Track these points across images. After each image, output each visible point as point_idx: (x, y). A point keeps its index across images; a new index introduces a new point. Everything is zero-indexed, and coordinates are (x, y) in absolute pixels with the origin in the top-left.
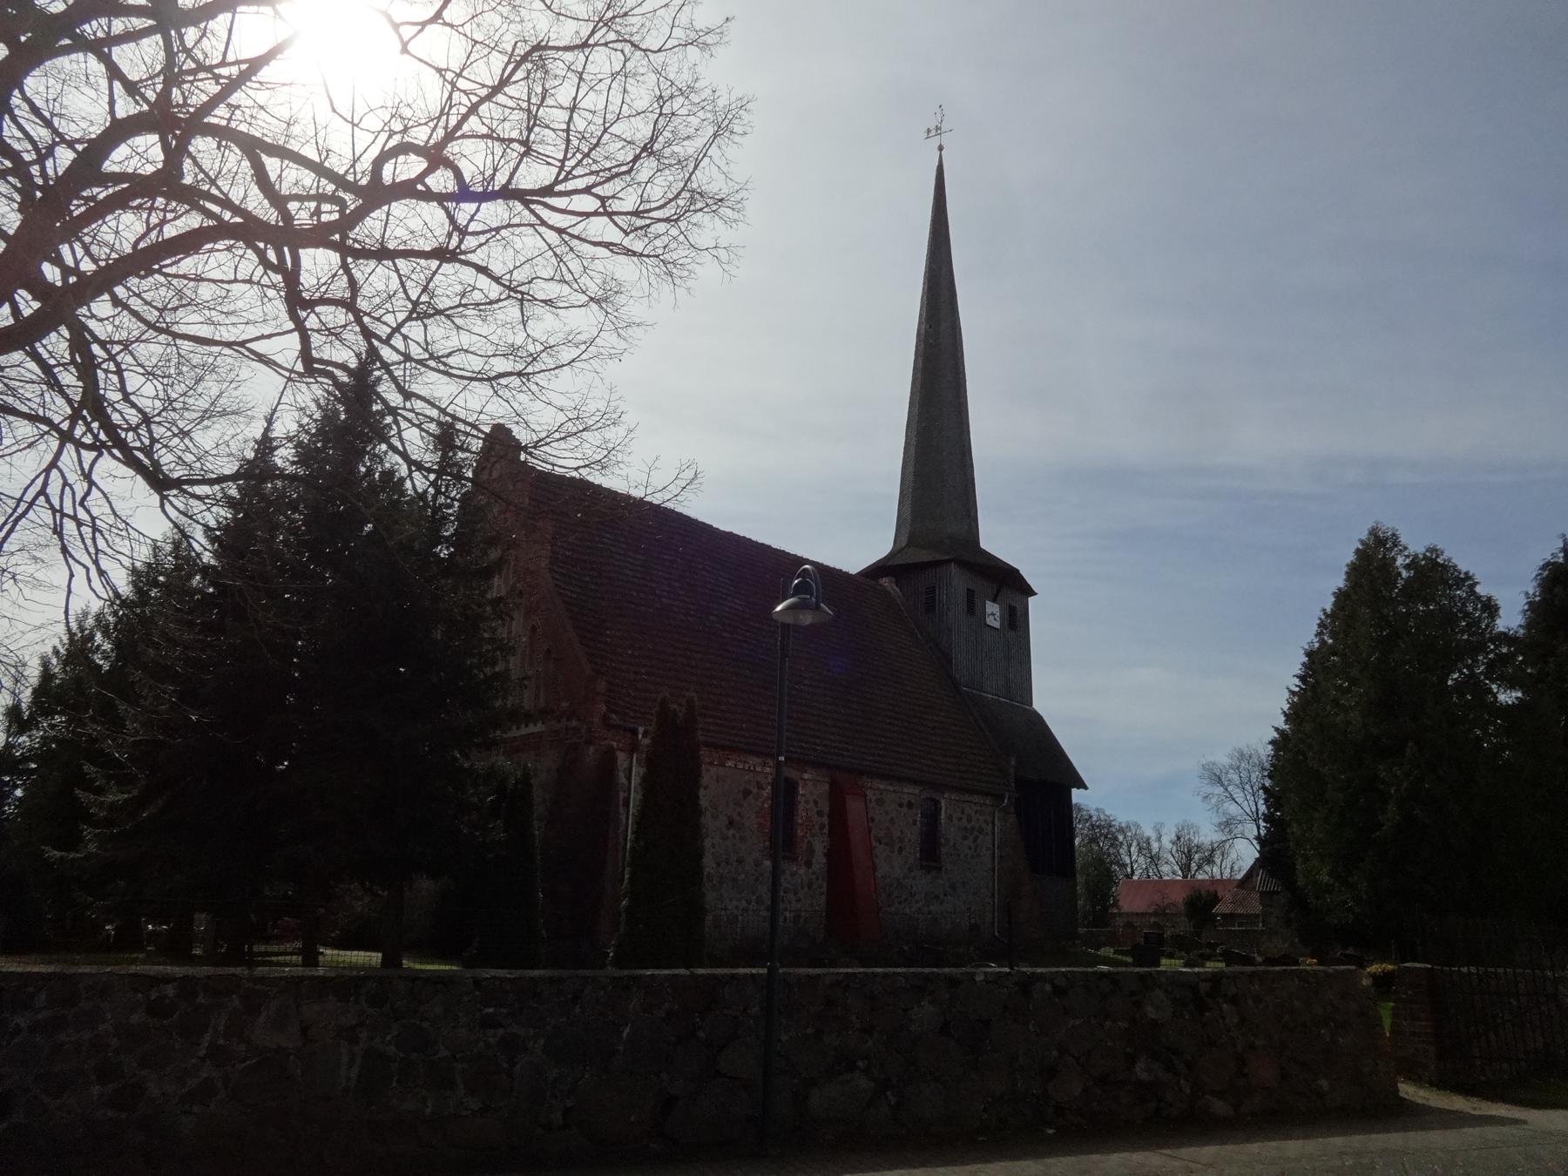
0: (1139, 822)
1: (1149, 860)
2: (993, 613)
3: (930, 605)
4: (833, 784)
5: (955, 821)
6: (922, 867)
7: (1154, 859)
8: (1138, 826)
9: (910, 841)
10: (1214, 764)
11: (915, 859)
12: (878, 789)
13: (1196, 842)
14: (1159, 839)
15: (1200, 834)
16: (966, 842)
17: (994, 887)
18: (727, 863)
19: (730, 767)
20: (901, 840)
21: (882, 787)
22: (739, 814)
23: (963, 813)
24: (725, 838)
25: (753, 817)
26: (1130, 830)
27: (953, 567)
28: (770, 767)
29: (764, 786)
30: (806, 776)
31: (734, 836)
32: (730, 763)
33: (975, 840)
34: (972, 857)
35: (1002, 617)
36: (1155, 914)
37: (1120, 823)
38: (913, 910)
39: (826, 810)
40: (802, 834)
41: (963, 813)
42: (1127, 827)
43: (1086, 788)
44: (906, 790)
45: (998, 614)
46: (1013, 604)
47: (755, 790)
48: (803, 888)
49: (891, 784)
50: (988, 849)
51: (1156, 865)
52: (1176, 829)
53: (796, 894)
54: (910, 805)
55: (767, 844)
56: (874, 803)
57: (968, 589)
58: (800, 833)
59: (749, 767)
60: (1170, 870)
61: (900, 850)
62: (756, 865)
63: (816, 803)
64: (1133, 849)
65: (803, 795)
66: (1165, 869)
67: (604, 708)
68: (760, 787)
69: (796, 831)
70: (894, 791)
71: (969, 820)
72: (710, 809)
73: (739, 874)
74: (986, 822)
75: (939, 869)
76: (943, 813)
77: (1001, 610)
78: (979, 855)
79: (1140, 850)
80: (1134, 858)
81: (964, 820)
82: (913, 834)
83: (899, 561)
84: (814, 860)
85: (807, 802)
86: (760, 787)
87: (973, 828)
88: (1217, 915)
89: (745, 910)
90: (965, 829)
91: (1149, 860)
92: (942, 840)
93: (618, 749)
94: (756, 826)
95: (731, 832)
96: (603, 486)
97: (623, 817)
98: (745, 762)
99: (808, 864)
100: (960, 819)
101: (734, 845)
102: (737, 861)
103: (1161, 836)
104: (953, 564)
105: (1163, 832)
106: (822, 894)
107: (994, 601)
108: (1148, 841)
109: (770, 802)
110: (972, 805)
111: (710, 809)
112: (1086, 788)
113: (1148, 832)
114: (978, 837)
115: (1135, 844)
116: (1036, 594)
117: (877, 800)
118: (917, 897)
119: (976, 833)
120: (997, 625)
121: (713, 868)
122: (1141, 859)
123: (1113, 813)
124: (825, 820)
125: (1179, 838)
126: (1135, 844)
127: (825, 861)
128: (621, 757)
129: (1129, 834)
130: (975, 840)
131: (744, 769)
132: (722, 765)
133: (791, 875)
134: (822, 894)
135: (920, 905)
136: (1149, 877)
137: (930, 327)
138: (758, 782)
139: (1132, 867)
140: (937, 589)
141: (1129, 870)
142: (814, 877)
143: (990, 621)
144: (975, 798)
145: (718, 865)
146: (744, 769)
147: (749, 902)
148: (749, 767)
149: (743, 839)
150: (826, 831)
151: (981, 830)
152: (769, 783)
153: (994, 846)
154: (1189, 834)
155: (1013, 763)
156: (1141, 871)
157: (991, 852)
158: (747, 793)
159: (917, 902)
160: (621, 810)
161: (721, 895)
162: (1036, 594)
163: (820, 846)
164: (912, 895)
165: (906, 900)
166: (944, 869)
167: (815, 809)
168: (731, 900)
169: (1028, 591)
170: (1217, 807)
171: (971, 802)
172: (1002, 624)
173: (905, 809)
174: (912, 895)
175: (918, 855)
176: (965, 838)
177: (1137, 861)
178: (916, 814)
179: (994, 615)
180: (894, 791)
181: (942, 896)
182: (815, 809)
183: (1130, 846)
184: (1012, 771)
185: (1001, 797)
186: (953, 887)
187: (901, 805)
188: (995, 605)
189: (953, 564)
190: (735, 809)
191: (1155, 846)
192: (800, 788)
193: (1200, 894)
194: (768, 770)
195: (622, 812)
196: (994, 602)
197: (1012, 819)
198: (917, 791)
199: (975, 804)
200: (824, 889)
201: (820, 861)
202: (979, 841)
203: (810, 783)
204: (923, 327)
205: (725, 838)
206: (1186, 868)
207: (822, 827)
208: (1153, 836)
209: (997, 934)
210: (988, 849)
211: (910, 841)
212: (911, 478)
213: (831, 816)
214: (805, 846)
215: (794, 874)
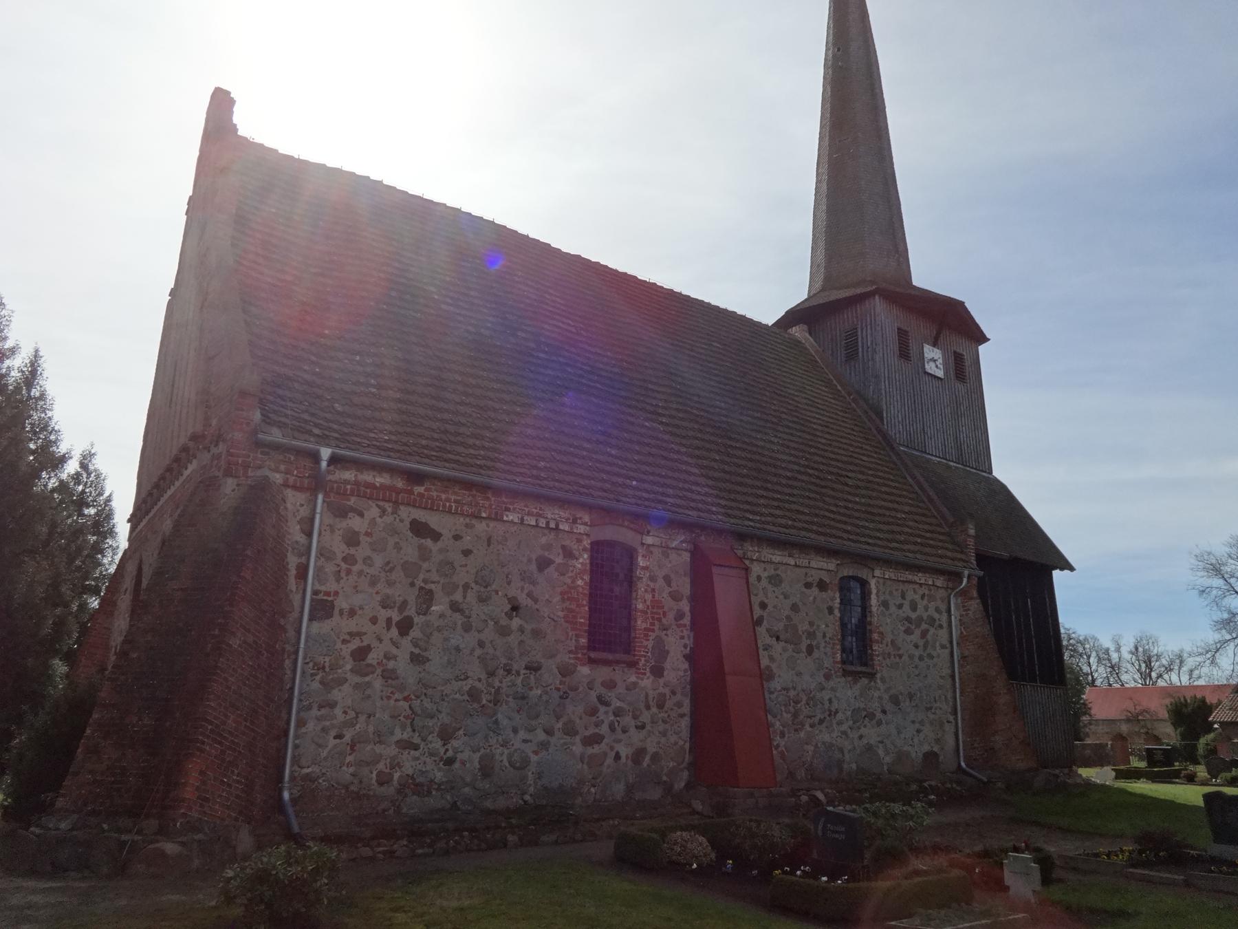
0: (1096, 635)
1: (1109, 670)
2: (934, 359)
3: (852, 352)
4: (697, 555)
5: (893, 609)
6: (846, 673)
7: (1114, 668)
8: (1096, 639)
9: (824, 636)
10: (1209, 554)
11: (835, 662)
12: (771, 562)
13: (1155, 652)
14: (1118, 650)
15: (1160, 644)
16: (909, 638)
17: (955, 698)
18: (509, 672)
19: (512, 522)
20: (811, 635)
21: (777, 559)
22: (529, 595)
23: (903, 597)
24: (504, 632)
25: (557, 599)
26: (1088, 642)
27: (878, 304)
28: (585, 524)
29: (576, 553)
30: (649, 540)
31: (521, 630)
32: (511, 517)
33: (924, 634)
34: (921, 658)
35: (945, 364)
36: (1128, 720)
37: (1079, 636)
38: (834, 735)
39: (686, 590)
40: (644, 626)
41: (903, 597)
42: (1084, 640)
43: (1072, 569)
44: (813, 564)
45: (940, 361)
46: (960, 351)
47: (559, 560)
48: (648, 707)
49: (790, 556)
50: (943, 647)
51: (1117, 674)
52: (1134, 640)
53: (635, 717)
54: (822, 586)
55: (583, 641)
56: (764, 582)
57: (898, 329)
58: (640, 624)
59: (548, 523)
60: (1130, 678)
61: (810, 650)
62: (563, 676)
63: (667, 580)
64: (1092, 660)
65: (646, 568)
66: (1124, 677)
67: (257, 416)
68: (568, 554)
69: (636, 622)
70: (796, 566)
71: (914, 607)
72: (473, 585)
73: (531, 689)
74: (937, 610)
75: (871, 676)
76: (873, 596)
77: (944, 356)
78: (931, 657)
79: (1099, 660)
80: (1094, 667)
81: (906, 607)
82: (829, 626)
83: (814, 302)
84: (667, 665)
85: (653, 579)
86: (568, 554)
87: (920, 619)
88: (1215, 723)
89: (544, 746)
90: (908, 619)
91: (1109, 670)
92: (875, 636)
93: (286, 485)
94: (561, 614)
95: (516, 622)
96: (385, 183)
97: (296, 599)
98: (540, 515)
99: (658, 672)
100: (900, 606)
101: (522, 642)
102: (527, 668)
103: (1120, 647)
104: (877, 297)
105: (1122, 643)
106: (682, 716)
107: (935, 344)
108: (1107, 651)
109: (587, 578)
110: (916, 586)
111: (473, 585)
112: (1072, 569)
113: (1106, 642)
114: (927, 631)
115: (1094, 654)
116: (989, 340)
117: (770, 578)
118: (840, 716)
119: (924, 626)
120: (940, 373)
121: (480, 680)
122: (1101, 669)
123: (1072, 627)
124: (685, 606)
125: (1137, 649)
126: (1094, 654)
127: (686, 666)
128: (294, 501)
129: (1087, 646)
130: (924, 634)
131: (537, 526)
132: (498, 518)
133: (628, 689)
134: (682, 716)
135: (844, 727)
136: (1110, 685)
137: (839, 50)
138: (563, 547)
139: (1092, 677)
140: (859, 330)
141: (1090, 678)
142: (667, 691)
143: (930, 368)
144: (920, 577)
145: (491, 674)
146: (537, 526)
147: (549, 732)
148: (548, 523)
149: (537, 634)
150: (687, 620)
151: (932, 621)
152: (585, 549)
153: (951, 642)
154: (1148, 644)
155: (972, 532)
156: (1102, 680)
157: (947, 651)
158: (543, 564)
159: (840, 723)
160: (292, 583)
161: (496, 722)
162: (989, 340)
163: (677, 644)
164: (832, 714)
165: (821, 721)
166: (878, 676)
167: (668, 590)
168: (515, 731)
169: (983, 339)
170: (1216, 602)
171: (915, 583)
172: (946, 373)
173: (815, 591)
174: (832, 714)
175: (839, 656)
176: (908, 632)
177: (1097, 671)
178: (833, 599)
179: (935, 361)
180: (796, 566)
181: (879, 715)
182: (668, 590)
183: (1089, 657)
184: (971, 542)
185: (957, 576)
186: (895, 700)
187: (808, 585)
188: (936, 350)
189: (877, 297)
190: (522, 589)
191: (1115, 656)
192: (640, 559)
193: (1186, 700)
194: (581, 529)
195: (294, 589)
196: (934, 346)
197: (975, 605)
198: (832, 566)
199: (921, 585)
200: (686, 708)
201: (677, 668)
202: (929, 637)
203: (657, 551)
204: (831, 51)
205: (504, 632)
206: (1146, 676)
207: (680, 616)
208: (1112, 648)
209: (963, 764)
210: (943, 647)
211: (824, 636)
212: (824, 216)
213: (693, 599)
214: (650, 644)
215: (632, 687)
